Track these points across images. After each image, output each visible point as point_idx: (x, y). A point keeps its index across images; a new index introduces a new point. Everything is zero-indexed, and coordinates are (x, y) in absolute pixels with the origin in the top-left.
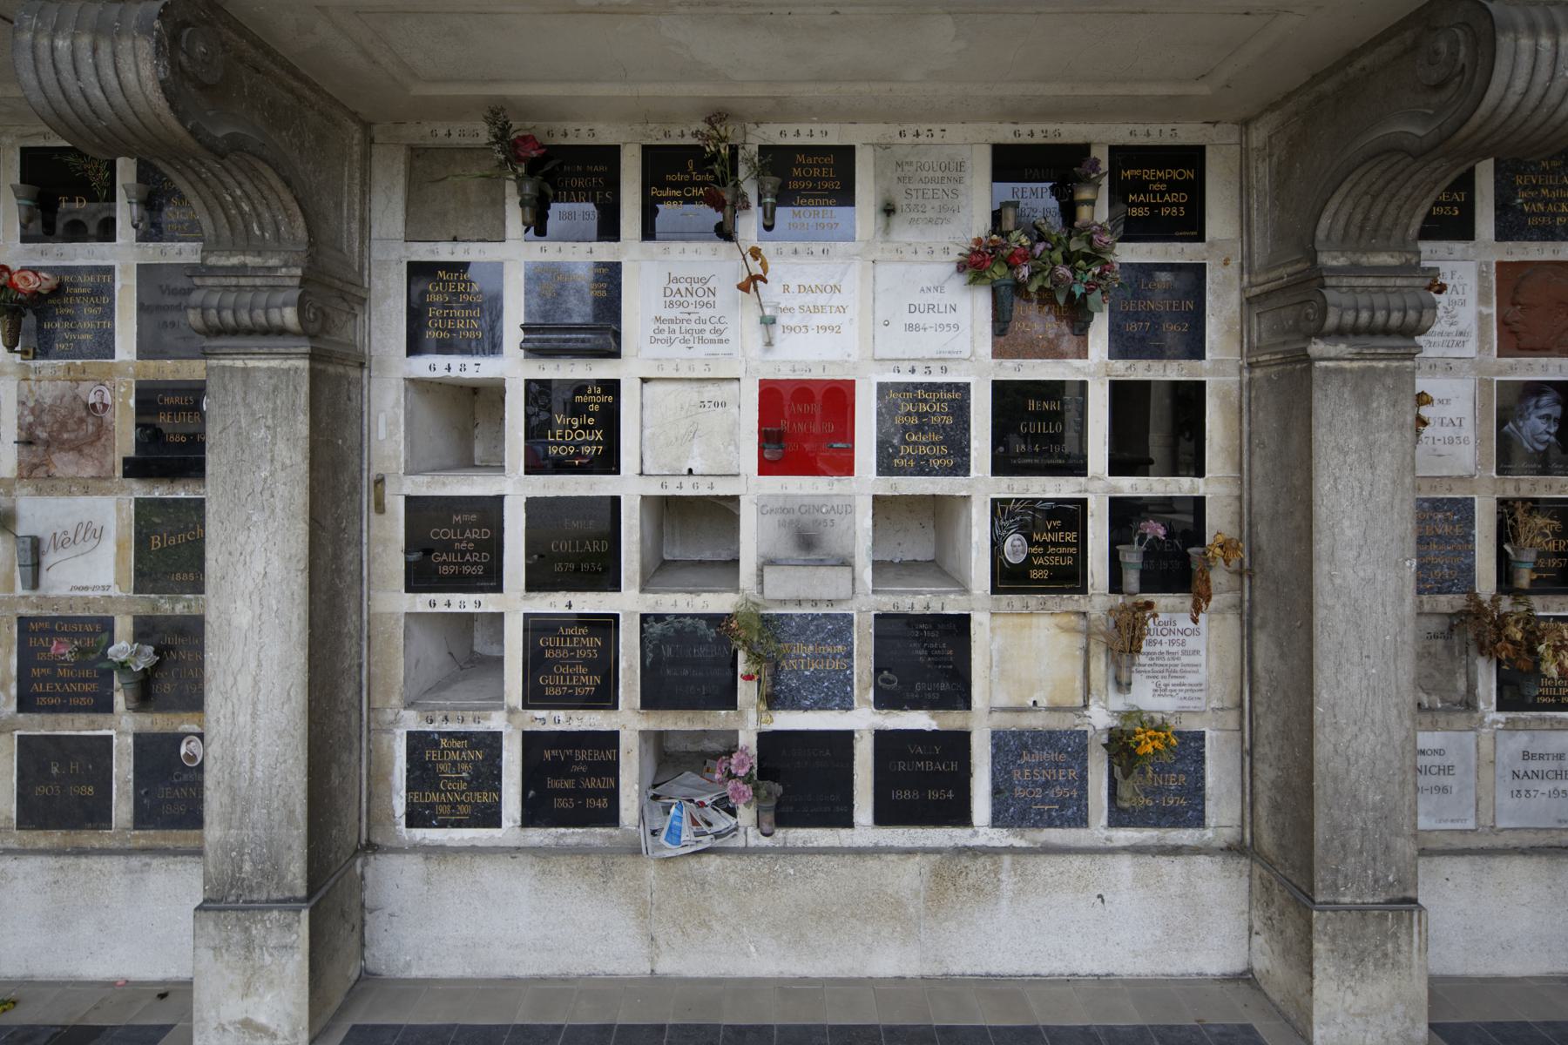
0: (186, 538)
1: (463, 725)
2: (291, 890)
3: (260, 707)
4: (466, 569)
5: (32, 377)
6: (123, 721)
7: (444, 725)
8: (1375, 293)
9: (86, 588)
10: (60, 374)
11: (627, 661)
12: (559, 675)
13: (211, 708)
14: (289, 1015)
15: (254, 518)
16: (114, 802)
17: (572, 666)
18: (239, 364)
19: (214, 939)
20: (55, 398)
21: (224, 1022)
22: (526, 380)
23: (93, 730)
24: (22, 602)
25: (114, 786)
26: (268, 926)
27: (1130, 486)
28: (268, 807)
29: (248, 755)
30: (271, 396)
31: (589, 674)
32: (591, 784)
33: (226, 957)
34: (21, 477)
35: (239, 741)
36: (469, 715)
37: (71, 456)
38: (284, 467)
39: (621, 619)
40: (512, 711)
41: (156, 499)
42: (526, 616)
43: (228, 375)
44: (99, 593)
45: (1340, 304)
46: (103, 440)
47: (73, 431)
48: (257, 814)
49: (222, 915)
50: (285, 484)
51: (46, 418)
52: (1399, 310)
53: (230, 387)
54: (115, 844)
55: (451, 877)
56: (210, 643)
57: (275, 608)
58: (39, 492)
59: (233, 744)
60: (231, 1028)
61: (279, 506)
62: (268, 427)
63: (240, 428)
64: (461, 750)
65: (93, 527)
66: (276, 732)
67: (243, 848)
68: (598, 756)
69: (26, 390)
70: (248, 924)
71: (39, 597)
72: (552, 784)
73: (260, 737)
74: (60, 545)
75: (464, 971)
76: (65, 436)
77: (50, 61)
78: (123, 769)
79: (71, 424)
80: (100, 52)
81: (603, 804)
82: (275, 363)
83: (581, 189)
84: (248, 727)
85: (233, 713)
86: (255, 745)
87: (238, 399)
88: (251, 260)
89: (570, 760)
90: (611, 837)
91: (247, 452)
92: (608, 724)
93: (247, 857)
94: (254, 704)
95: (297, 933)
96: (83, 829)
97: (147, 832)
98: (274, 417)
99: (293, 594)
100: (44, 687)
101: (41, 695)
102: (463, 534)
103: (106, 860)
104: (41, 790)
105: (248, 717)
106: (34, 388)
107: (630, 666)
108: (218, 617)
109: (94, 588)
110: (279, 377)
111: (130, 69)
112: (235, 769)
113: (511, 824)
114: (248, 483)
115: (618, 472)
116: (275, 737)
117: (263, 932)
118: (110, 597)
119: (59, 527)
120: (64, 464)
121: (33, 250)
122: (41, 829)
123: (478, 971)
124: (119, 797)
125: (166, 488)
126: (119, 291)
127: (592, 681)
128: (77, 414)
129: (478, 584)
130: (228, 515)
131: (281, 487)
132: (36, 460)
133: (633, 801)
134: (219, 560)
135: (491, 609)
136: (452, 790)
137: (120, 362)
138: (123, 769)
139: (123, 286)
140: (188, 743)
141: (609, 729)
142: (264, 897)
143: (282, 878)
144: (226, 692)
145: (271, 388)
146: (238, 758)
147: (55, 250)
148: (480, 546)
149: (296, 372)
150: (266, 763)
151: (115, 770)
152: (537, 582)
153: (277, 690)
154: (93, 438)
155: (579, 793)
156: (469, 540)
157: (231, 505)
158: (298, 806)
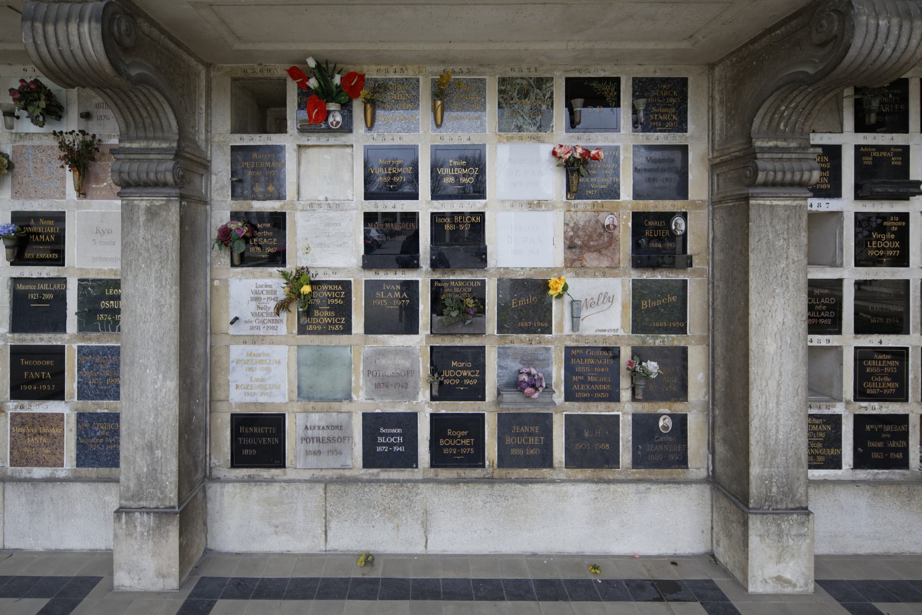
0: (662, 302)
1: (820, 411)
2: (799, 502)
3: (781, 399)
4: (822, 321)
5: (573, 209)
6: (626, 407)
7: (809, 410)
8: (786, 161)
9: (605, 331)
10: (589, 208)
11: (914, 374)
12: (875, 382)
13: (753, 399)
14: (803, 574)
15: (777, 291)
16: (621, 453)
17: (882, 377)
18: (768, 203)
19: (760, 531)
20: (585, 222)
21: (766, 578)
22: (855, 213)
23: (609, 412)
24: (568, 338)
25: (621, 444)
26: (791, 523)
27: (409, 276)
28: (786, 455)
29: (775, 426)
30: (786, 221)
31: (892, 381)
32: (893, 444)
33: (767, 540)
34: (566, 267)
35: (769, 418)
36: (823, 404)
37: (595, 255)
38: (794, 262)
39: (910, 350)
40: (848, 403)
41: (644, 280)
42: (856, 348)
43: (761, 209)
44: (612, 333)
45: (766, 167)
46: (613, 246)
47: (596, 240)
48: (780, 459)
49: (765, 517)
50: (794, 271)
51: (580, 233)
52: (799, 171)
53: (763, 216)
54: (622, 477)
55: (822, 497)
56: (753, 362)
57: (789, 342)
58: (577, 275)
59: (766, 420)
60: (770, 581)
61: (791, 284)
62: (784, 239)
63: (769, 239)
64: (819, 425)
65: (608, 295)
66: (790, 413)
67: (772, 479)
68: (897, 429)
69: (569, 217)
70: (779, 522)
71: (577, 335)
72: (871, 444)
73: (781, 416)
74: (589, 306)
75: (830, 551)
76: (592, 243)
77: (874, 32)
78: (626, 434)
79: (595, 236)
80: (903, 28)
81: (899, 456)
82: (788, 203)
83: (887, 103)
84: (774, 410)
85: (766, 402)
86: (779, 420)
87: (768, 223)
88: (781, 144)
89: (881, 431)
90: (904, 475)
91: (773, 253)
92: (903, 411)
93: (774, 484)
94: (778, 397)
95: (808, 527)
96: (602, 468)
97: (640, 470)
98: (788, 233)
99: (799, 334)
100: (580, 387)
101: (578, 391)
102: (819, 301)
103: (625, 486)
104: (579, 446)
105: (775, 404)
106: (574, 216)
107: (915, 377)
108: (757, 347)
109: (610, 330)
110: (791, 210)
111: (916, 38)
112: (767, 434)
113: (848, 467)
114: (774, 271)
115: (908, 266)
116: (790, 416)
117: (788, 527)
118: (618, 336)
119: (589, 295)
120: (591, 259)
121: (573, 137)
122: (579, 468)
123: (837, 551)
124: (623, 450)
125: (650, 273)
126: (623, 160)
127: (893, 385)
128: (598, 231)
129: (828, 330)
130: (762, 289)
131: (792, 274)
132: (575, 257)
133: (917, 455)
134: (758, 315)
135: (835, 344)
136: (814, 448)
137: (623, 201)
138: (626, 434)
139: (625, 158)
140: (664, 419)
141: (903, 413)
142: (784, 507)
143: (794, 496)
144: (762, 390)
145: (786, 217)
146: (769, 427)
147: (585, 137)
148: (829, 308)
149: (800, 208)
150: (785, 431)
151: (621, 435)
152: (861, 328)
153: (791, 389)
154: (608, 245)
155: (886, 450)
156: (823, 304)
157: (764, 283)
158: (803, 455)
